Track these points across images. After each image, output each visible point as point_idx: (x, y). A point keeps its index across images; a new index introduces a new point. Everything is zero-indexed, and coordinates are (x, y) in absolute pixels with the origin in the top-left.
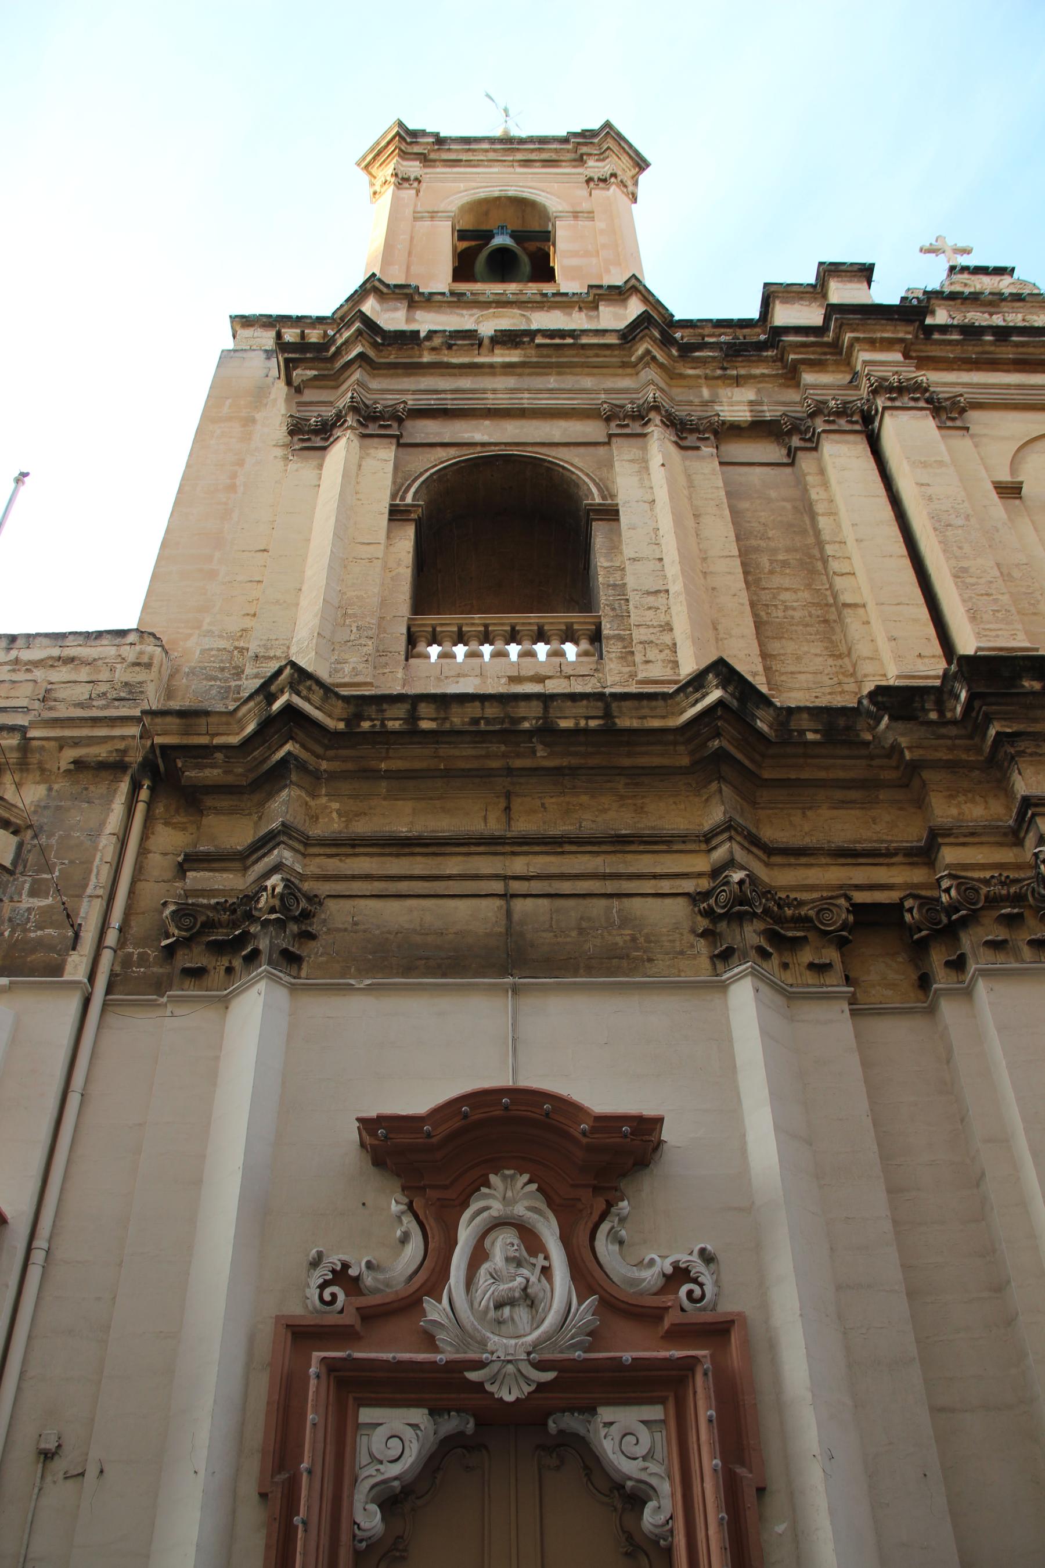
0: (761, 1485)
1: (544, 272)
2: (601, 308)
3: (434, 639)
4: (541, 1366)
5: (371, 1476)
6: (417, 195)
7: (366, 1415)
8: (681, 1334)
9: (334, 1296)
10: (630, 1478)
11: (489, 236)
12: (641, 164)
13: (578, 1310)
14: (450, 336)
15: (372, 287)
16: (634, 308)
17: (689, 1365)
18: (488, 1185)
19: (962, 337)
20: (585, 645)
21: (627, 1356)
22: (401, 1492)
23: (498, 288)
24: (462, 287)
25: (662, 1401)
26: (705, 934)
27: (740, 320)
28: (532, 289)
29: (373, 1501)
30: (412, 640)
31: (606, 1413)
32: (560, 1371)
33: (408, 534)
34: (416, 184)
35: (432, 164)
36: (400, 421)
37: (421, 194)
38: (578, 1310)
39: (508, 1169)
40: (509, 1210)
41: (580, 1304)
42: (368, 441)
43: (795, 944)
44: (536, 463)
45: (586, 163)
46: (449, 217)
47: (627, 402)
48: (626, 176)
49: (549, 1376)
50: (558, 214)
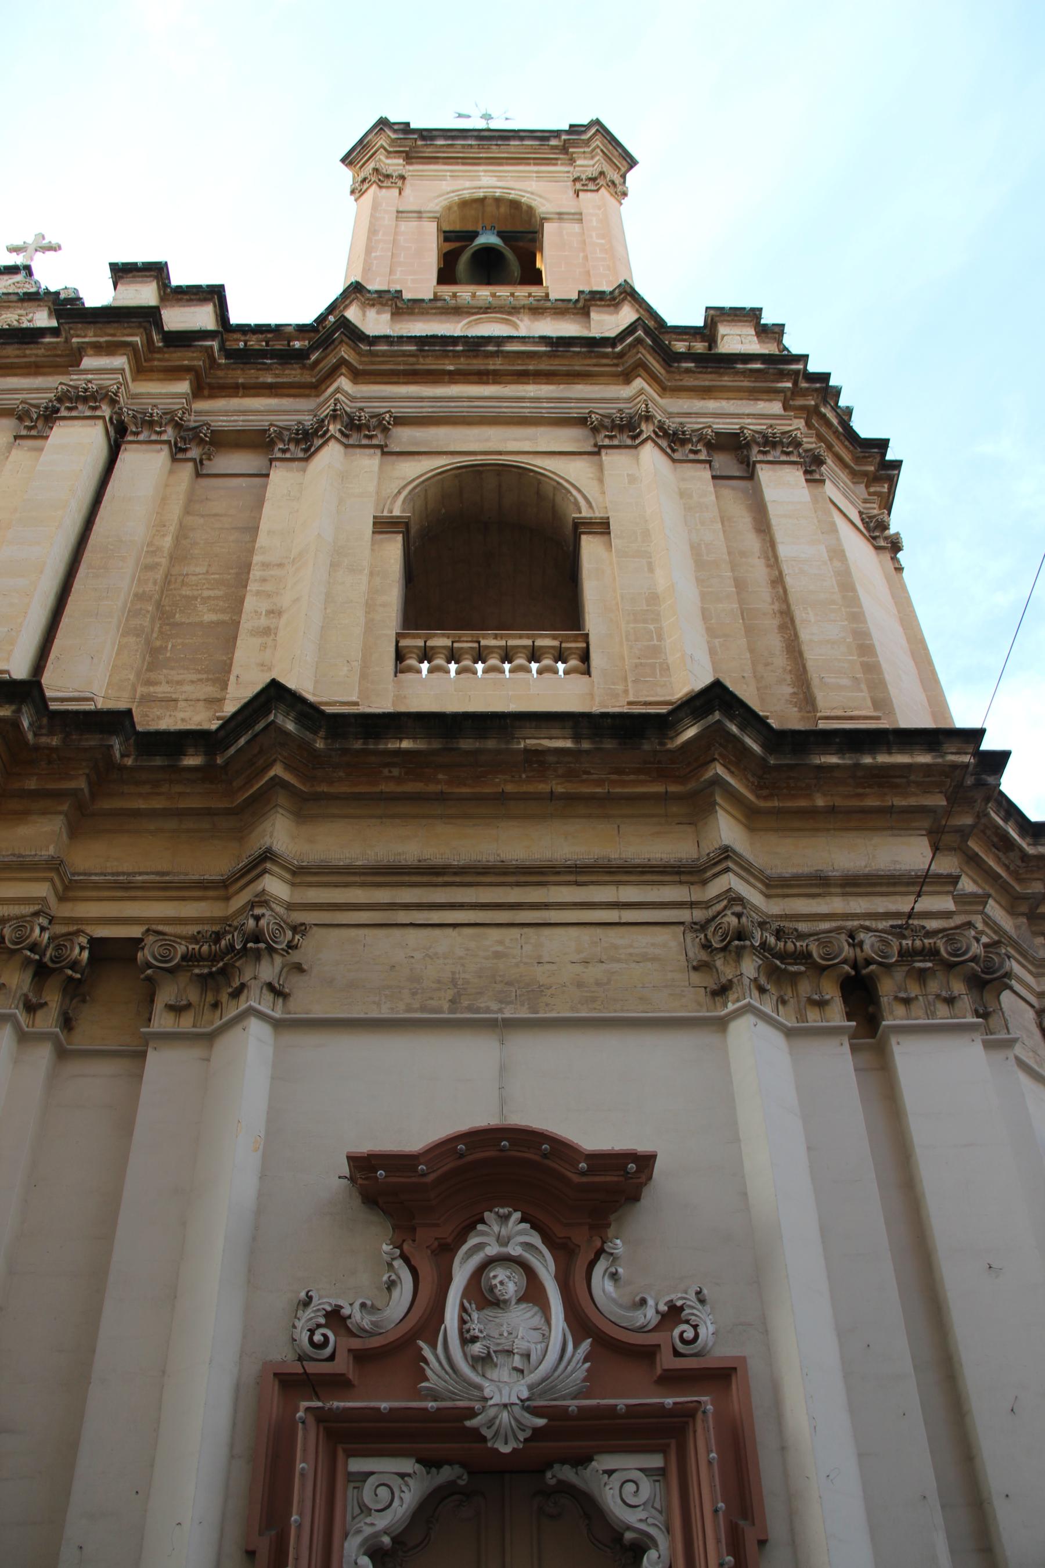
0: (762, 1538)
1: (534, 277)
2: (593, 315)
3: (426, 655)
4: (536, 1412)
5: (613, 1495)
6: (400, 193)
7: (357, 1465)
8: (672, 1380)
9: (324, 1335)
10: (629, 1528)
11: (473, 235)
12: (632, 163)
13: (573, 1356)
14: (556, 343)
15: (355, 291)
16: (627, 315)
17: (688, 1414)
18: (482, 1221)
19: (548, 349)
20: (574, 662)
21: (621, 1403)
22: (393, 1543)
23: (484, 293)
24: (447, 291)
25: (663, 1450)
26: (699, 967)
27: (257, 326)
28: (522, 293)
29: (365, 1554)
30: (400, 656)
31: (604, 1462)
32: (550, 1420)
33: (394, 549)
34: (400, 183)
35: (554, 162)
36: (385, 430)
37: (405, 193)
38: (573, 1356)
39: (503, 1207)
40: (504, 1250)
41: (576, 1346)
42: (350, 450)
43: (794, 979)
44: (522, 472)
45: (575, 162)
46: (435, 218)
47: (614, 411)
48: (613, 175)
49: (541, 1422)
50: (548, 216)
